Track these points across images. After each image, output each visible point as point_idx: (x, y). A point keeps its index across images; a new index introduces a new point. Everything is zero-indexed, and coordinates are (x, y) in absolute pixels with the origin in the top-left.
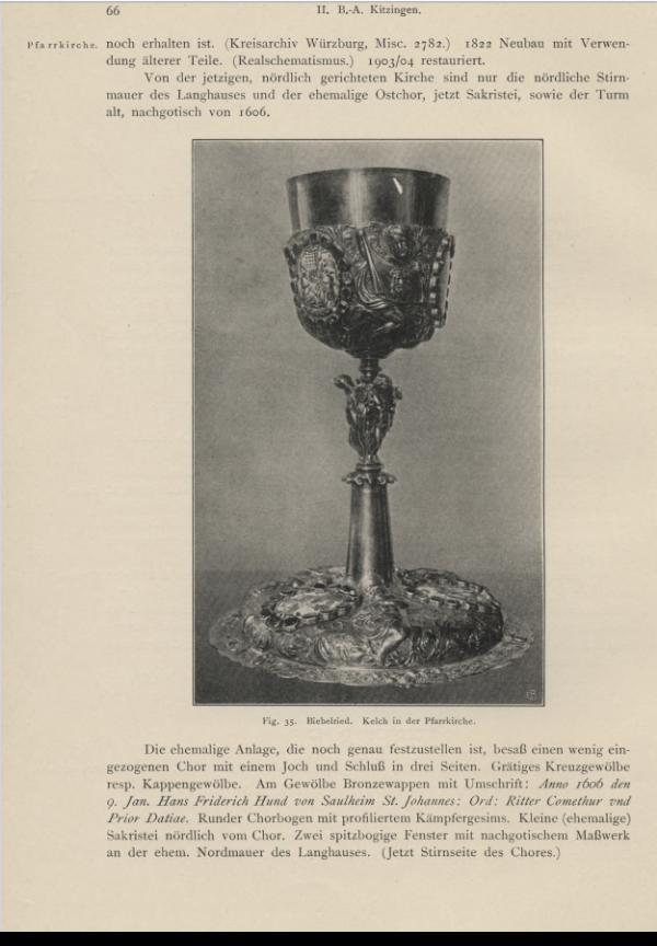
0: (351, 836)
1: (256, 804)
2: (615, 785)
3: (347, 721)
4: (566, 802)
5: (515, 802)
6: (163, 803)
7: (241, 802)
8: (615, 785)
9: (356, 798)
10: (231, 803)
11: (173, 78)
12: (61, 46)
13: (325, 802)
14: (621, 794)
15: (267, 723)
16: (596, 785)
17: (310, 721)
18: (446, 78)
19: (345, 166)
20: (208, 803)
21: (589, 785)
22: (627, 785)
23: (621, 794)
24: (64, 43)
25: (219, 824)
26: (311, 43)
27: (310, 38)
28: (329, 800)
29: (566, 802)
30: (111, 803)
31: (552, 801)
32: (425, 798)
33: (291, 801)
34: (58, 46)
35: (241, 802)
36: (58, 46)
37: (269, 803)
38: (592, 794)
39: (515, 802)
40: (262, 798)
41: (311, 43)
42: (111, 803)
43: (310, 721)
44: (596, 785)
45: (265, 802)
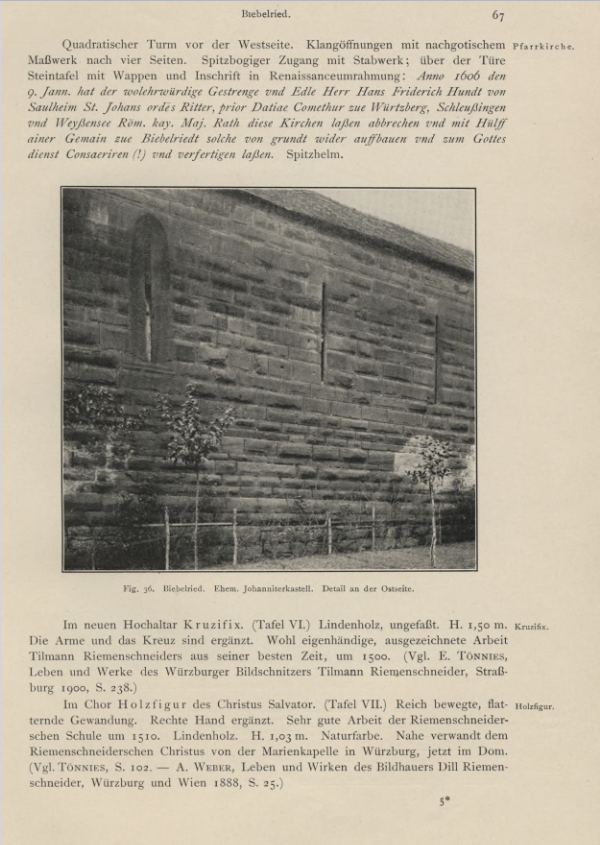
0: (308, 155)
1: (449, 95)
2: (492, 77)
3: (200, 589)
4: (312, 108)
5: (189, 108)
6: (362, 93)
7: (435, 93)
8: (492, 77)
9: (59, 105)
10: (426, 93)
11: (234, 752)
12: (541, 48)
13: (32, 109)
14: (497, 85)
15: (128, 590)
16: (474, 77)
17: (166, 588)
18: (180, 657)
19: (216, 394)
20: (405, 93)
21: (467, 77)
22: (503, 77)
23: (497, 85)
24: (544, 44)
25: (347, 645)
26: (243, 44)
27: (242, 40)
28: (444, 107)
29: (312, 108)
30: (31, 93)
31: (299, 107)
32: (124, 105)
33: (448, 124)
34: (539, 48)
35: (435, 93)
36: (539, 48)
37: (461, 93)
38: (334, 100)
39: (189, 108)
40: (454, 89)
41: (243, 44)
42: (31, 93)
43: (166, 588)
44: (474, 77)
45: (457, 93)
